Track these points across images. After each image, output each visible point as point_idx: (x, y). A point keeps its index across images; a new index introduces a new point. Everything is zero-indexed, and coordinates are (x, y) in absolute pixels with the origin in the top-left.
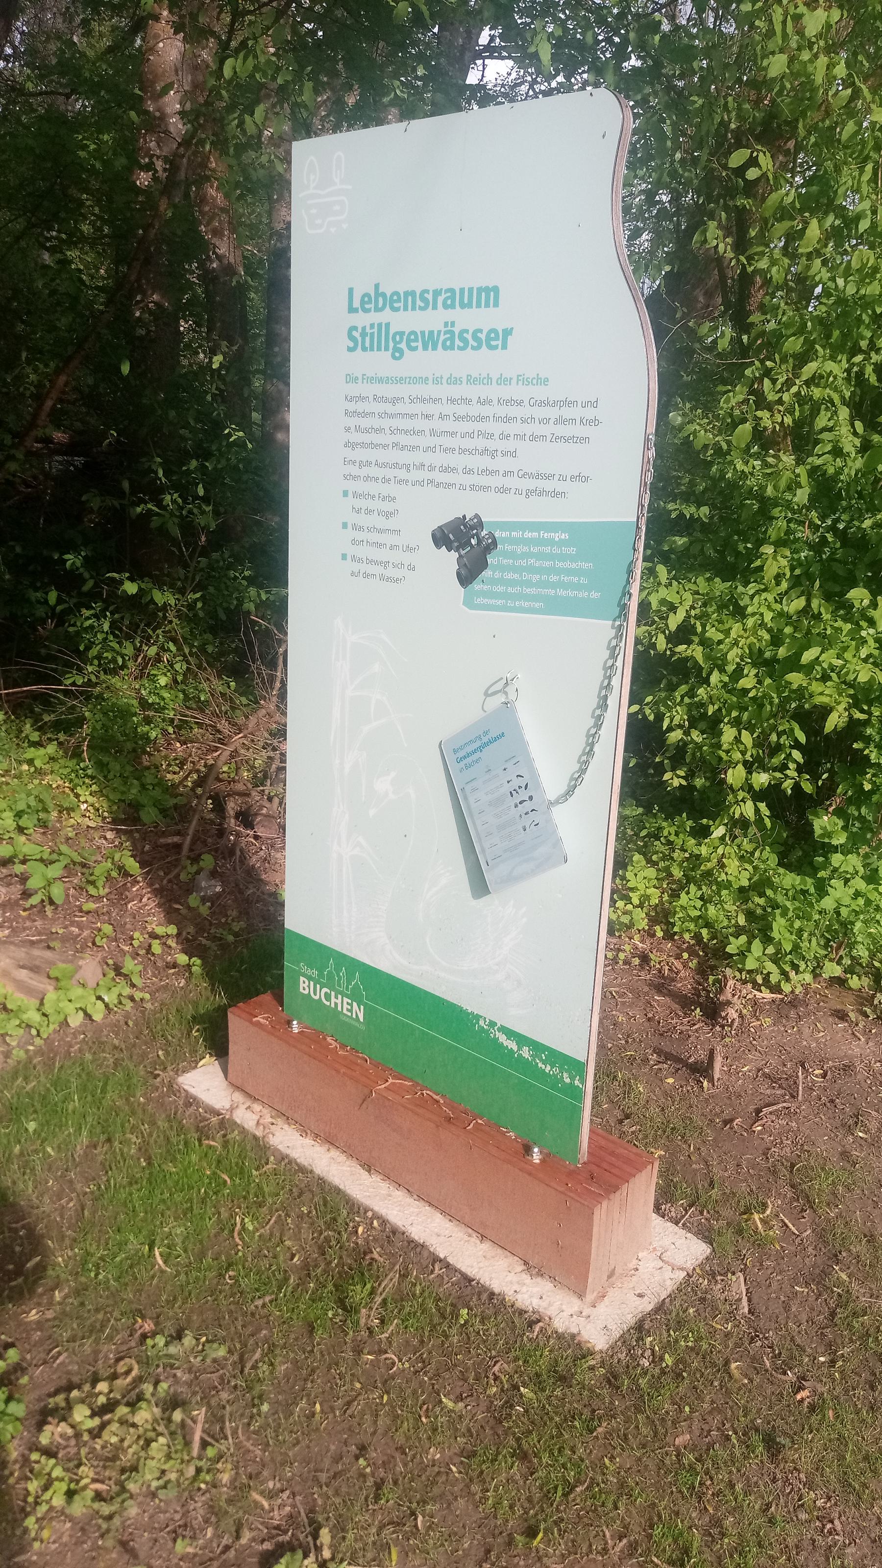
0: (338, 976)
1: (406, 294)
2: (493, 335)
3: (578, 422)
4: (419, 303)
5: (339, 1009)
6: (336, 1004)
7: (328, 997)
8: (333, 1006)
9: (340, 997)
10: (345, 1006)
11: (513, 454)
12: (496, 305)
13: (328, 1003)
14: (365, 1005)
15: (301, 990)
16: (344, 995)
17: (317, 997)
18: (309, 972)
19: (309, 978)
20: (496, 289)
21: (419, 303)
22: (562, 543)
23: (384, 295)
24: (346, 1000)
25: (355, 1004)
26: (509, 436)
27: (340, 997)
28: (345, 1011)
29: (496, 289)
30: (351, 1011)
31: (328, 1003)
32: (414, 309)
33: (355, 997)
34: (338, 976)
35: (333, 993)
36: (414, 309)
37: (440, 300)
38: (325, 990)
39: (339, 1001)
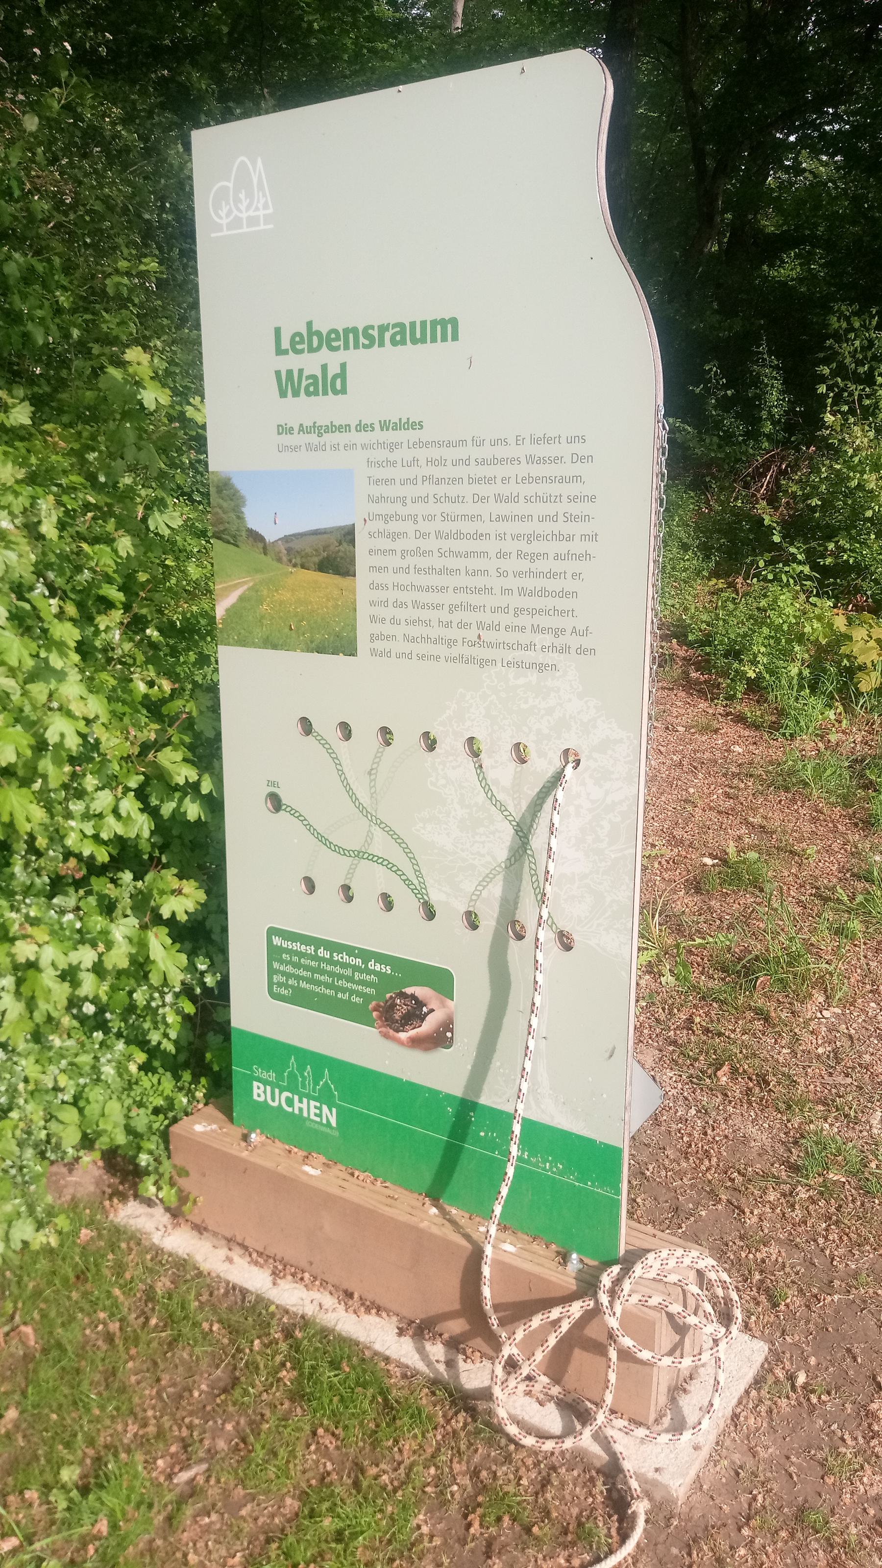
5: (305, 1114)
6: (301, 1109)
8: (297, 1111)
10: (313, 1111)
13: (290, 1110)
15: (255, 1097)
16: (309, 1097)
19: (265, 1083)
21: (362, 340)
23: (319, 334)
25: (325, 1108)
33: (325, 1098)
35: (296, 1098)
37: (387, 336)
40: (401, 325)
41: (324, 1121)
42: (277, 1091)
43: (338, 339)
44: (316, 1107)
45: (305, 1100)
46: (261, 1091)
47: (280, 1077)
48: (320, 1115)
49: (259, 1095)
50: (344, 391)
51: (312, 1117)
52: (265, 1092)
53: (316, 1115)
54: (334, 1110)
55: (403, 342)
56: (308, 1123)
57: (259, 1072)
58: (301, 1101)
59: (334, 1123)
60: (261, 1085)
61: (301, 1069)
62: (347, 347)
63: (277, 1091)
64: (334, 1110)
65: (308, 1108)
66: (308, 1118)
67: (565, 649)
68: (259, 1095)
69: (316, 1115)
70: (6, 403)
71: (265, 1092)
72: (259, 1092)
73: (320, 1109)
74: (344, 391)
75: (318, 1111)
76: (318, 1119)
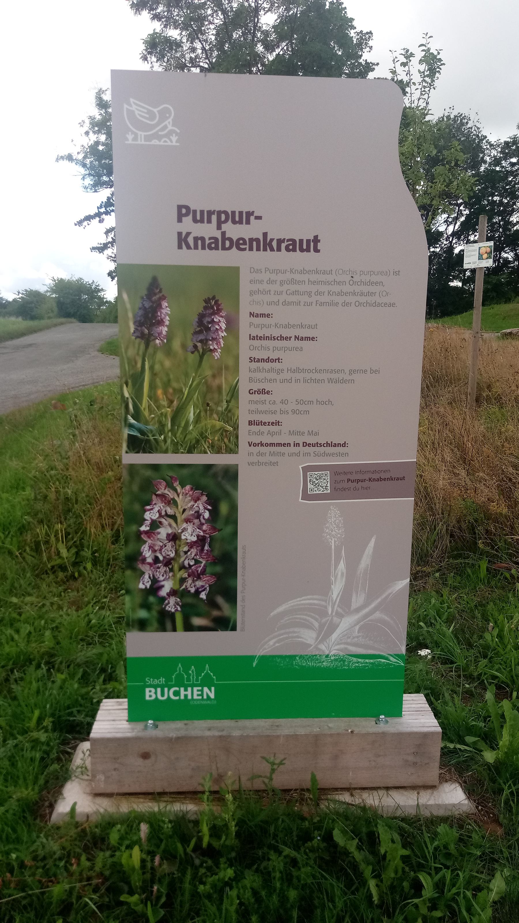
1: (251, 240)
2: (241, 242)
5: (190, 697)
6: (186, 696)
8: (182, 697)
10: (196, 693)
13: (177, 698)
15: (147, 698)
16: (193, 686)
19: (155, 687)
23: (231, 240)
25: (206, 689)
33: (207, 682)
35: (182, 689)
36: (203, 248)
37: (283, 246)
40: (294, 241)
41: (205, 697)
42: (166, 689)
43: (245, 243)
44: (198, 691)
45: (189, 689)
46: (152, 694)
47: (168, 679)
48: (202, 695)
49: (150, 696)
50: (180, 207)
51: (195, 697)
52: (156, 693)
53: (198, 695)
54: (213, 689)
55: (294, 250)
56: (191, 703)
57: (149, 681)
58: (186, 690)
59: (212, 696)
60: (153, 690)
61: (186, 671)
62: (251, 249)
63: (166, 689)
65: (193, 693)
66: (192, 699)
67: (277, 303)
68: (150, 696)
69: (198, 695)
70: (235, 799)
71: (156, 693)
72: (150, 694)
73: (202, 691)
74: (180, 207)
75: (200, 693)
76: (200, 697)
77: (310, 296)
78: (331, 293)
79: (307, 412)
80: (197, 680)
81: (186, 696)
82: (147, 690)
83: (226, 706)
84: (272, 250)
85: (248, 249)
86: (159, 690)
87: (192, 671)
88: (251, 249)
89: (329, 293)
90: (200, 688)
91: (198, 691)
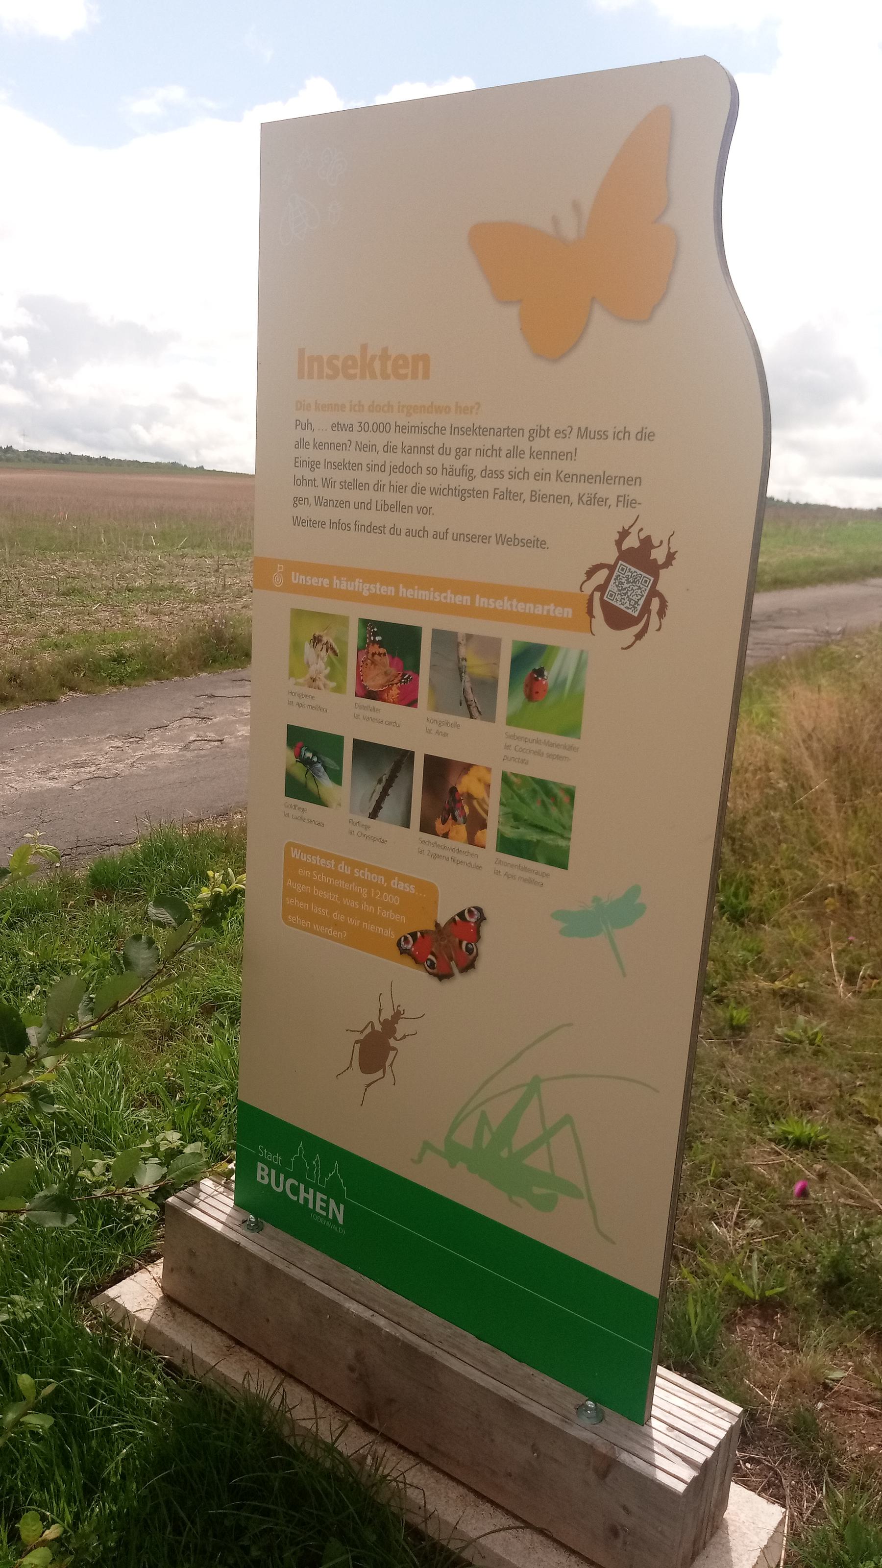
0: (310, 1164)
2: (401, 362)
3: (554, 477)
4: (327, 371)
5: (311, 1206)
6: (306, 1200)
7: (295, 1190)
8: (301, 1201)
9: (311, 1191)
10: (319, 1203)
11: (425, 510)
12: (426, 376)
13: (295, 1198)
14: (345, 1203)
15: (259, 1179)
16: (317, 1189)
17: (280, 1190)
18: (270, 1157)
19: (270, 1165)
20: (425, 358)
22: (710, 1510)
24: (319, 1195)
25: (332, 1203)
26: (423, 489)
27: (311, 1191)
28: (318, 1210)
29: (425, 358)
30: (326, 1209)
31: (295, 1198)
32: (320, 376)
33: (332, 1191)
34: (310, 1164)
35: (302, 1186)
36: (320, 376)
38: (291, 1181)
39: (310, 1197)
41: (331, 1217)
44: (322, 1200)
46: (265, 1174)
49: (263, 1178)
52: (269, 1175)
54: (342, 1206)
58: (307, 1191)
64: (342, 1206)
65: (314, 1200)
71: (269, 1175)
76: (324, 1214)
77: (471, 478)
78: (562, 476)
79: (445, 735)
80: (322, 1182)
81: (306, 1200)
82: (260, 1165)
83: (346, 1246)
84: (373, 376)
85: (410, 375)
86: (273, 1172)
87: (317, 1162)
88: (415, 376)
89: (558, 476)
90: (325, 1198)
91: (322, 1200)
